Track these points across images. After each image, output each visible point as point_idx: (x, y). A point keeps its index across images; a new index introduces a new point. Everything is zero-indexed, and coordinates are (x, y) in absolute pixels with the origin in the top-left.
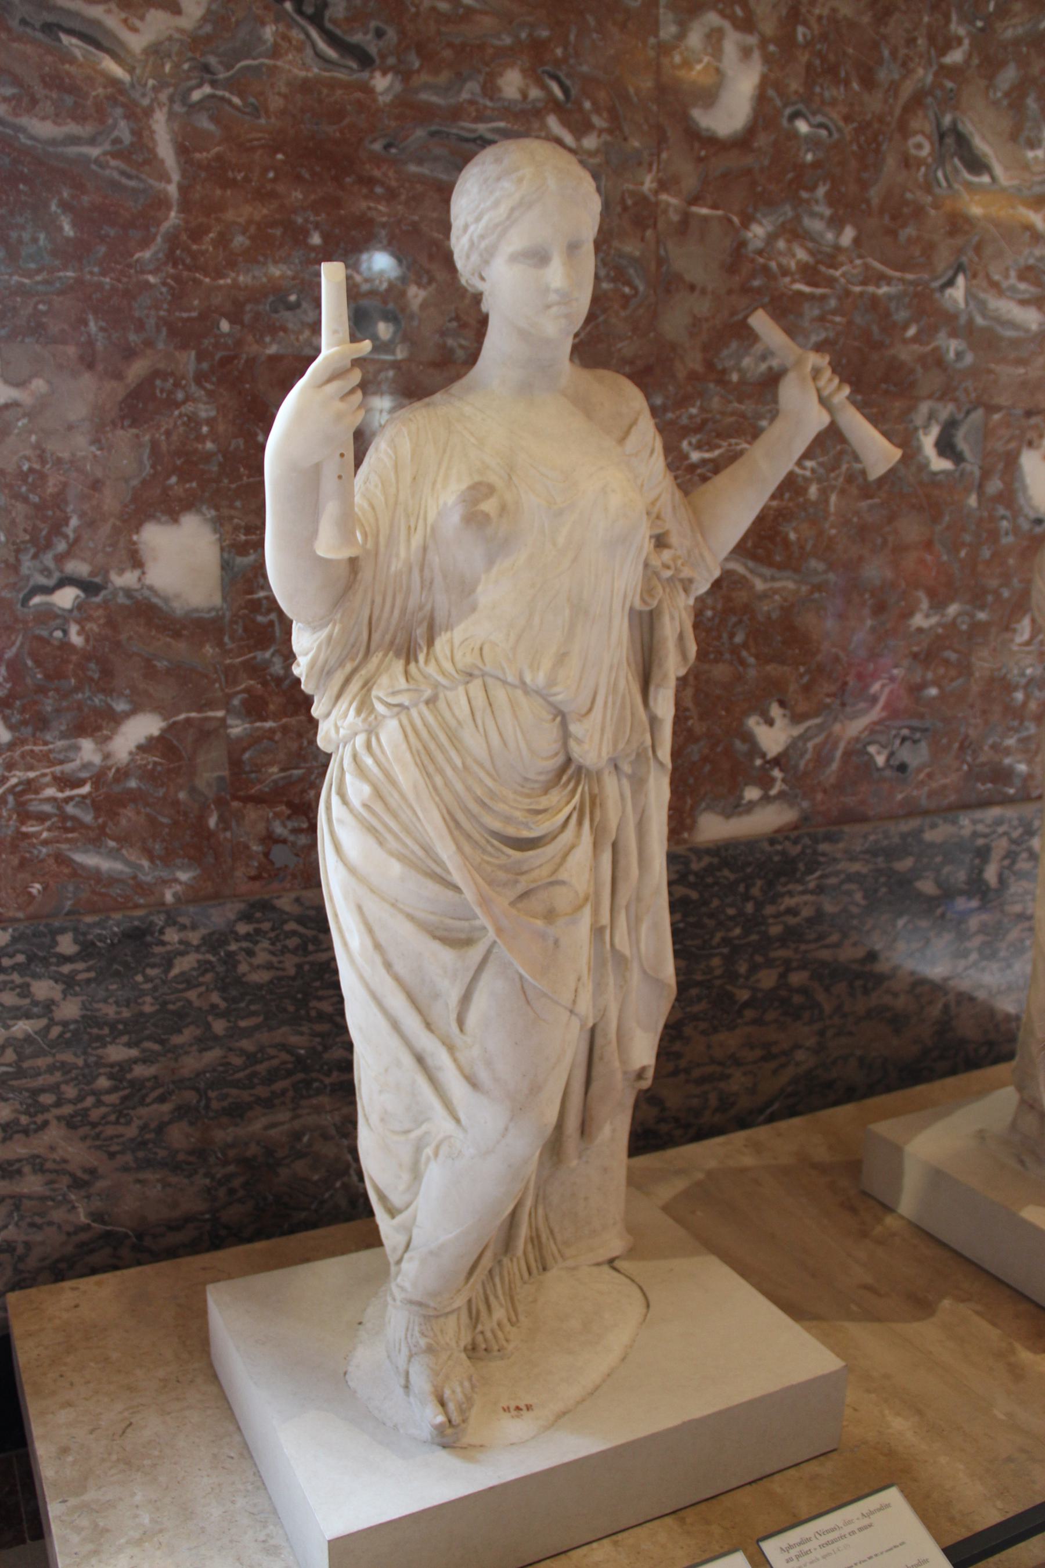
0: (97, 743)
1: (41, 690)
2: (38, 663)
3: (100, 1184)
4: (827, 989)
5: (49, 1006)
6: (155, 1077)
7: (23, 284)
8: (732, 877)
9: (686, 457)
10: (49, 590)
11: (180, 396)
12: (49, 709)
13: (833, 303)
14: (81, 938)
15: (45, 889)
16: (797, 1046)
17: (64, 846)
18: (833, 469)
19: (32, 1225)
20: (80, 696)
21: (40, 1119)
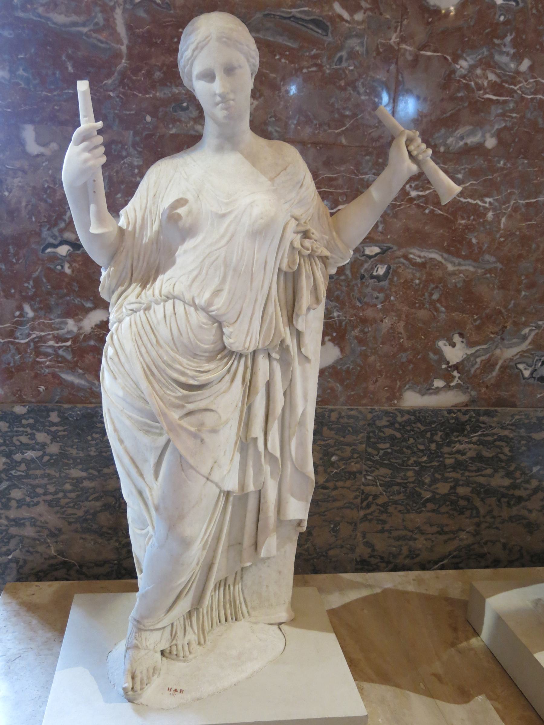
0: (75, 322)
1: (49, 294)
2: (49, 281)
3: (63, 537)
4: (482, 500)
5: (43, 446)
6: (94, 488)
7: (48, 96)
8: (423, 428)
9: (408, 194)
10: (55, 246)
11: (124, 154)
12: (53, 303)
13: (511, 105)
14: (61, 415)
15: (46, 389)
16: (461, 530)
17: (56, 370)
18: (504, 203)
19: (28, 551)
20: (68, 298)
21: (36, 500)
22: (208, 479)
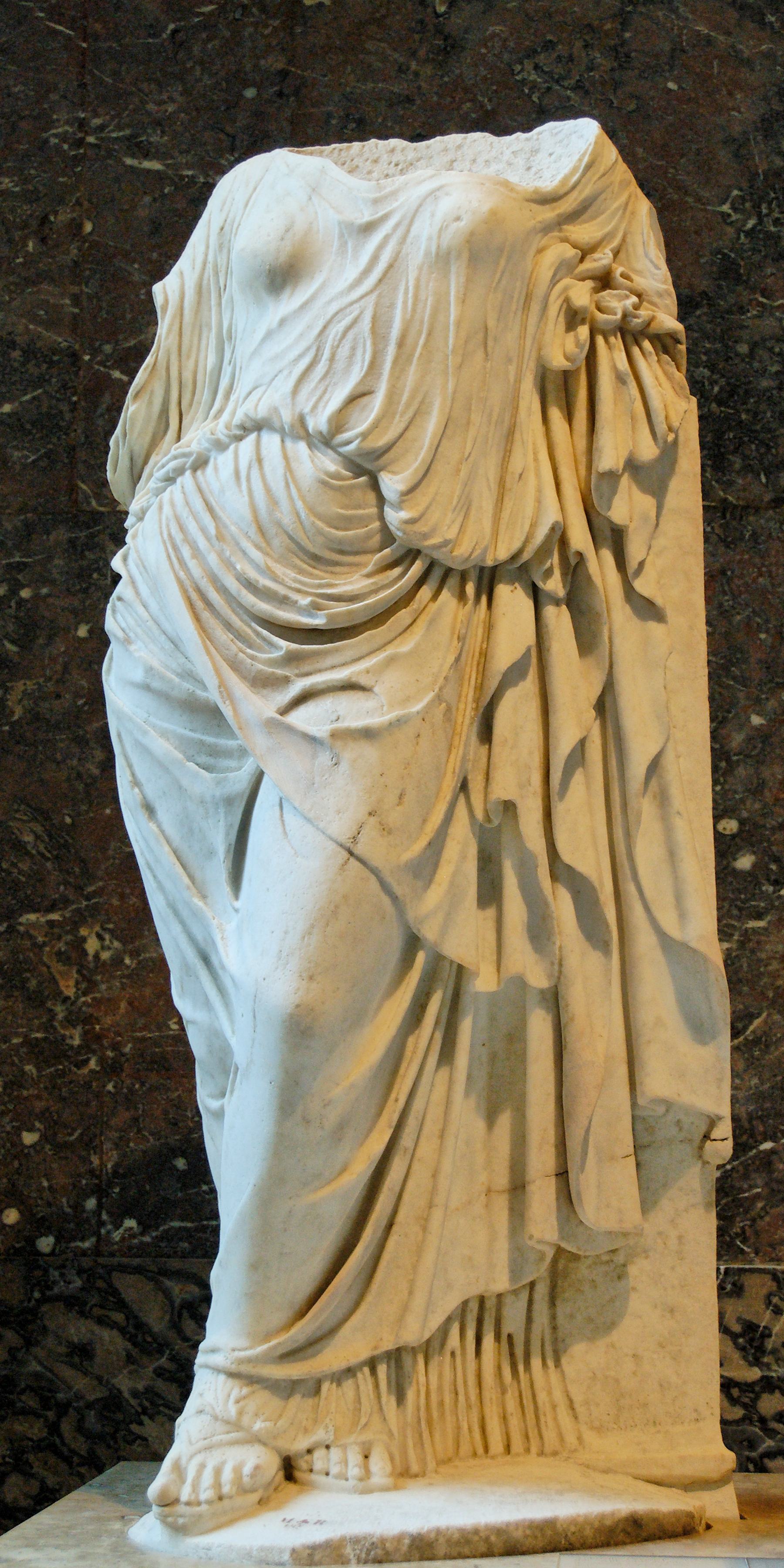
22: (351, 853)
